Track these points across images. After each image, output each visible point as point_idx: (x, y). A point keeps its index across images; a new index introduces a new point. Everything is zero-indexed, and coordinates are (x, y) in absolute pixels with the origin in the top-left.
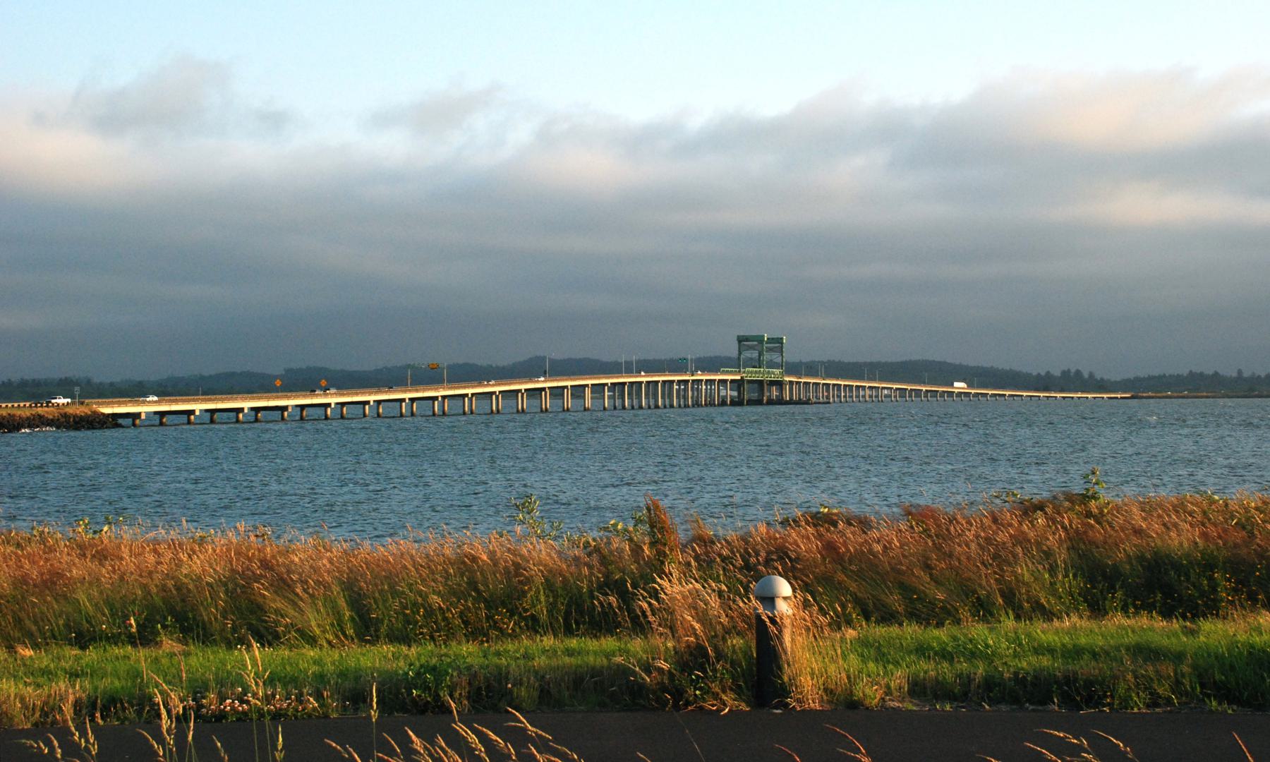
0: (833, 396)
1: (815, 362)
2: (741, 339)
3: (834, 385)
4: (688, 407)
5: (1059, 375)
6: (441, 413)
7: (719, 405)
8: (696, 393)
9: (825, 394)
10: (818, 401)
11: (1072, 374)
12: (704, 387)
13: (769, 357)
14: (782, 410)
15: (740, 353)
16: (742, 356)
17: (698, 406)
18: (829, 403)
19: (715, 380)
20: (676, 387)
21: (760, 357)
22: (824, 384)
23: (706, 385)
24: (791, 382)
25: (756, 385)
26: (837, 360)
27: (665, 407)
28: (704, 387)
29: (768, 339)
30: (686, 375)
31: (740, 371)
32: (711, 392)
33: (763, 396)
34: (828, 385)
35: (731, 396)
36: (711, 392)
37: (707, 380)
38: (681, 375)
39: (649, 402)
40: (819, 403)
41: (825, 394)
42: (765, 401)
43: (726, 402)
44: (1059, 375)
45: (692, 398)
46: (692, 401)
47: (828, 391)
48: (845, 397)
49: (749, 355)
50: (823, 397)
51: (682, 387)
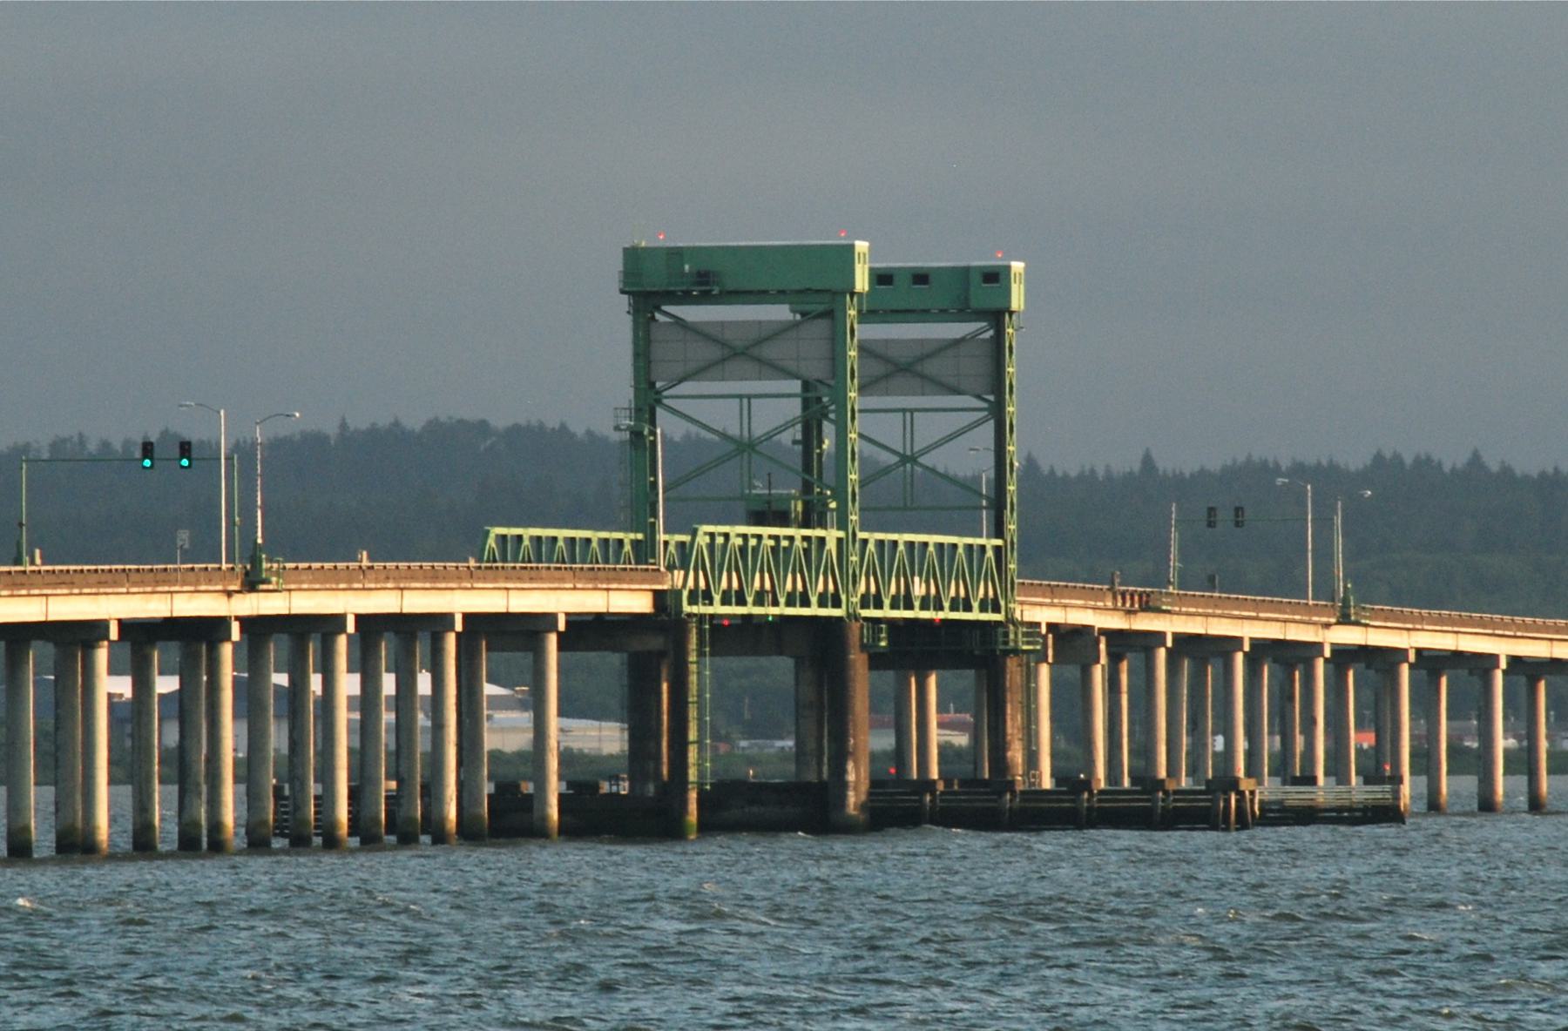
0: (1424, 761)
1: (1266, 471)
2: (656, 280)
3: (1431, 663)
4: (217, 846)
5: (1536, 476)
6: (125, 843)
7: (469, 832)
8: (277, 737)
9: (1358, 740)
10: (1296, 795)
11: (1101, 479)
12: (348, 684)
13: (889, 430)
14: (637, 875)
15: (648, 401)
16: (667, 426)
17: (299, 842)
18: (1387, 813)
19: (441, 621)
20: (113, 685)
21: (810, 435)
22: (1344, 656)
23: (365, 666)
24: (1071, 641)
25: (780, 669)
26: (1452, 457)
27: (143, 844)
28: (348, 684)
29: (881, 278)
30: (194, 582)
31: (644, 551)
32: (403, 727)
33: (840, 757)
34: (1381, 660)
35: (568, 759)
36: (403, 727)
37: (130, 628)
38: (157, 581)
39: (142, 806)
40: (1307, 815)
41: (1358, 740)
42: (853, 800)
43: (531, 803)
44: (1536, 476)
45: (248, 772)
46: (252, 797)
47: (1380, 716)
48: (1522, 762)
49: (724, 416)
50: (1337, 767)
51: (165, 684)
